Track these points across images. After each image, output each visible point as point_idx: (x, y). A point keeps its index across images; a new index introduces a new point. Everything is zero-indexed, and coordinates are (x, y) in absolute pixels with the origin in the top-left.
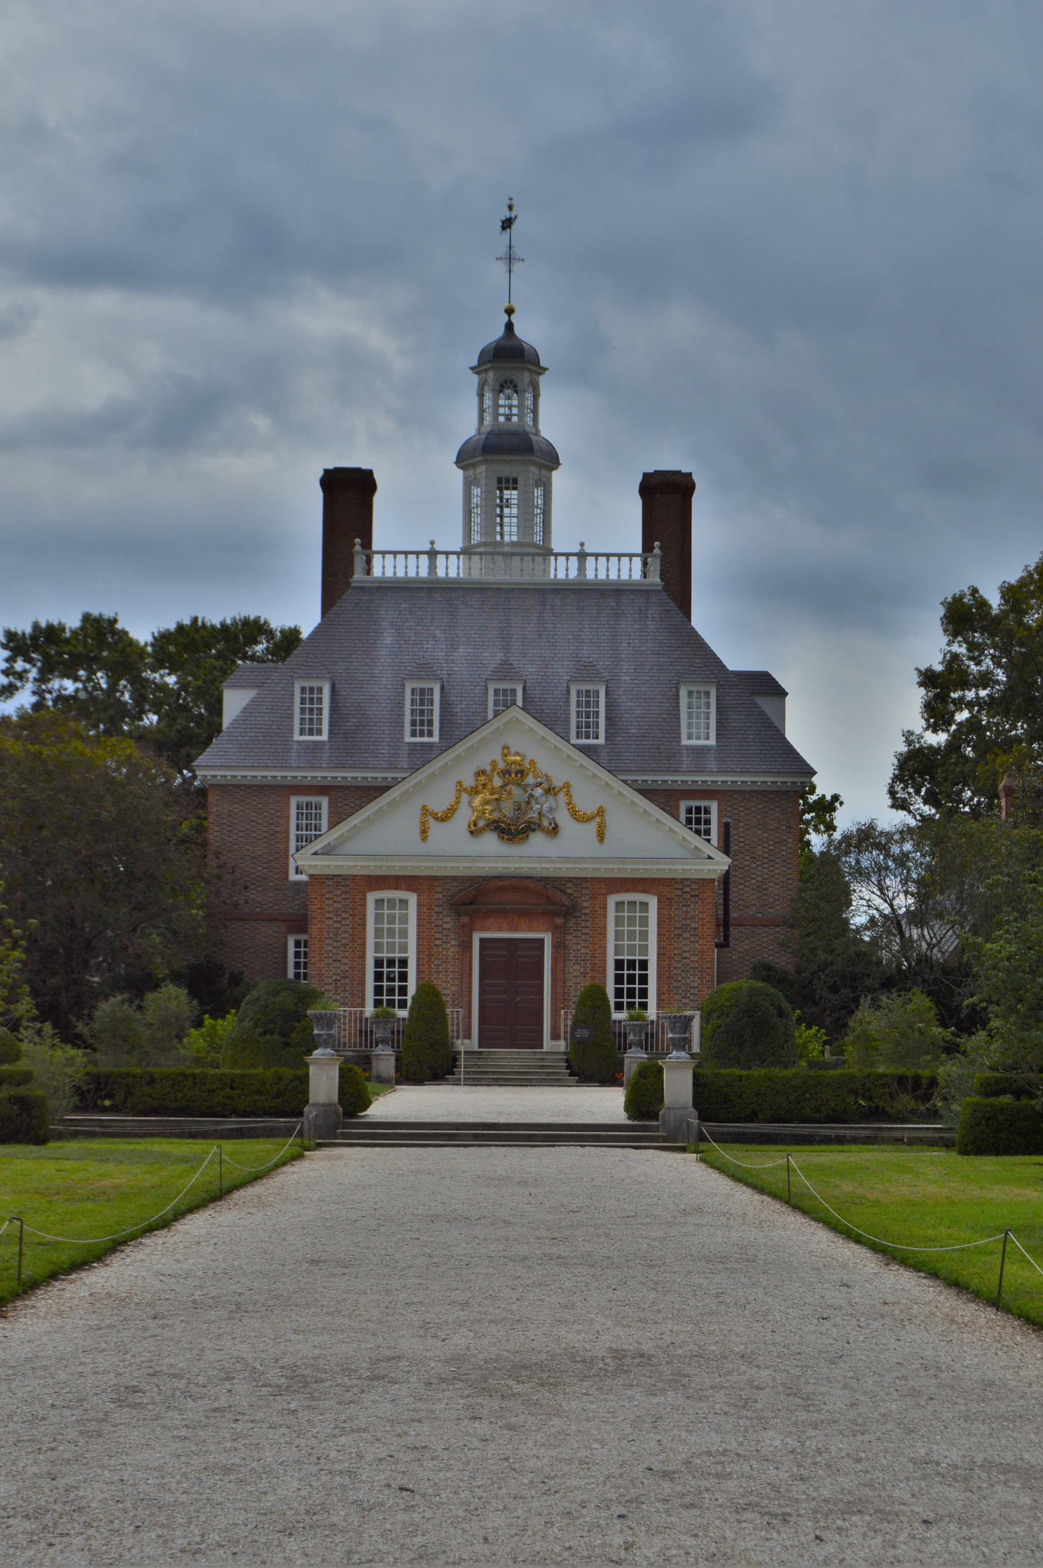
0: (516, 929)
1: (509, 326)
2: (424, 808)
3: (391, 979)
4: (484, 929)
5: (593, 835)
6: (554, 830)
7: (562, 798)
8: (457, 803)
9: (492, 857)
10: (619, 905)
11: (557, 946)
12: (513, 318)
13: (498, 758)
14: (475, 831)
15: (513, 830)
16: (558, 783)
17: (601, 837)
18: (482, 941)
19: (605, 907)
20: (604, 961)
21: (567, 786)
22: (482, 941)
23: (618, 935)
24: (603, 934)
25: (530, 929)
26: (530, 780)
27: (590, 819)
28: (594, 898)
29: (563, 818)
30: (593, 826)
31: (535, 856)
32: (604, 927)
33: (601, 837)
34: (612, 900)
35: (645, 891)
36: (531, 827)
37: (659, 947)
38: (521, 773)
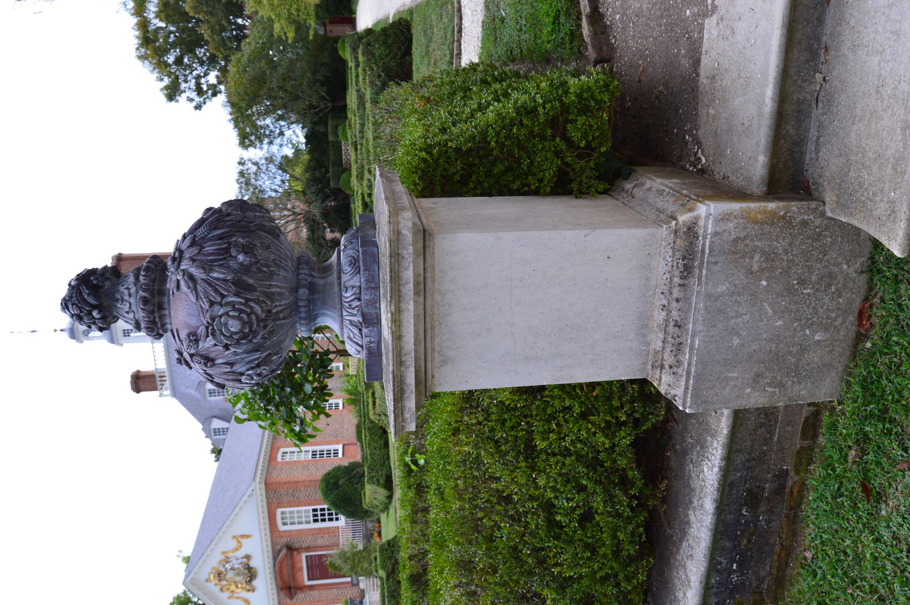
0: (301, 569)
1: (62, 330)
2: (234, 537)
3: (301, 517)
4: (303, 580)
5: (248, 540)
6: (248, 557)
7: (230, 555)
8: (239, 598)
9: (265, 582)
10: (284, 524)
11: (308, 549)
12: (58, 329)
13: (212, 584)
14: (253, 590)
15: (251, 574)
16: (222, 557)
17: (247, 536)
18: (309, 579)
19: (286, 532)
20: (314, 529)
21: (223, 553)
22: (309, 579)
23: (299, 512)
24: (300, 531)
25: (301, 562)
26: (222, 569)
27: (239, 541)
28: (282, 537)
29: (241, 553)
30: (243, 541)
31: (262, 562)
32: (297, 531)
33: (247, 536)
34: (282, 528)
35: (275, 515)
36: (249, 568)
37: (305, 505)
38: (219, 574)
